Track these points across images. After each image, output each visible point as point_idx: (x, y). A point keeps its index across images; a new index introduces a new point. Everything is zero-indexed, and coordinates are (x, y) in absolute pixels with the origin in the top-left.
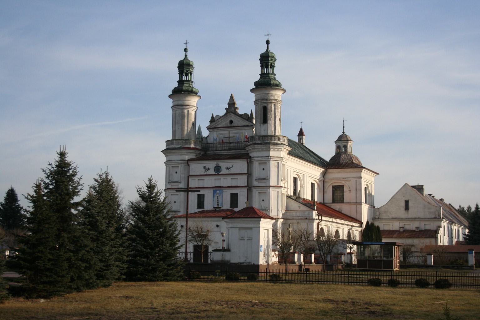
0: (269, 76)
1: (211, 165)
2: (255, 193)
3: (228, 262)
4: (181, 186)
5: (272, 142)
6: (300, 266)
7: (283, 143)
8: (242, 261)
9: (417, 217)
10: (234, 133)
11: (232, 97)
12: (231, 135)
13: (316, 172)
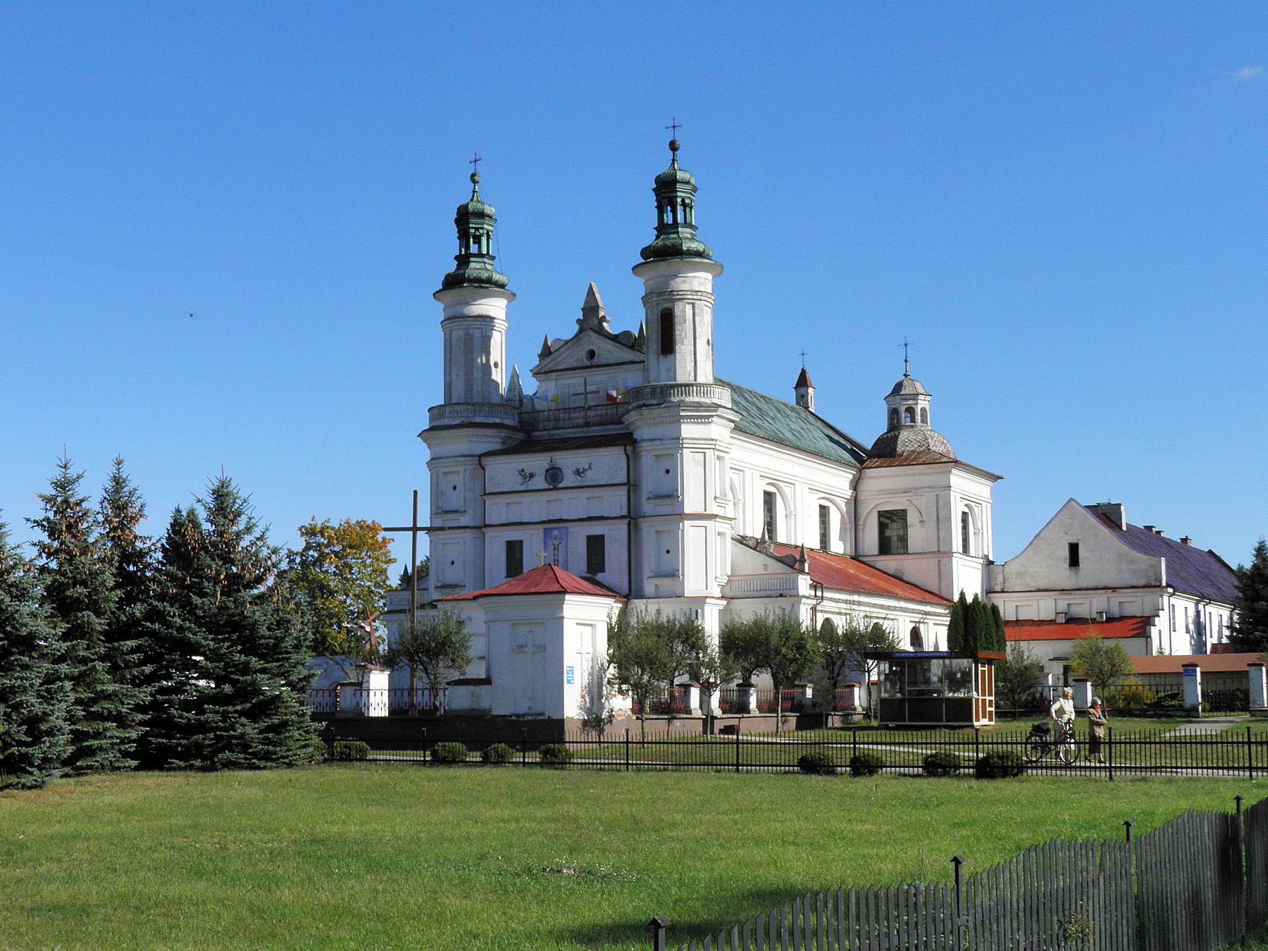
0: (677, 233)
1: (537, 463)
2: (647, 528)
3: (486, 712)
4: (464, 520)
5: (687, 399)
6: (709, 720)
7: (716, 401)
8: (522, 708)
9: (1102, 584)
10: (599, 380)
11: (591, 292)
12: (589, 389)
13: (838, 481)
